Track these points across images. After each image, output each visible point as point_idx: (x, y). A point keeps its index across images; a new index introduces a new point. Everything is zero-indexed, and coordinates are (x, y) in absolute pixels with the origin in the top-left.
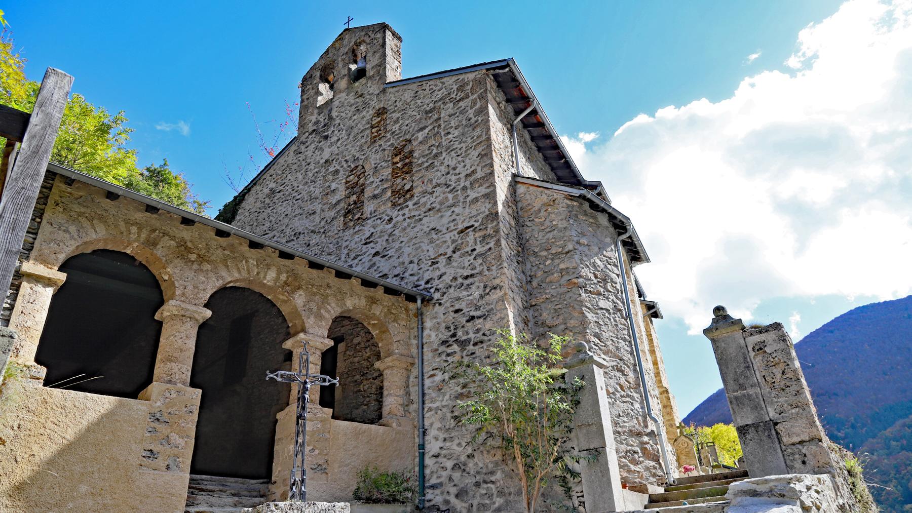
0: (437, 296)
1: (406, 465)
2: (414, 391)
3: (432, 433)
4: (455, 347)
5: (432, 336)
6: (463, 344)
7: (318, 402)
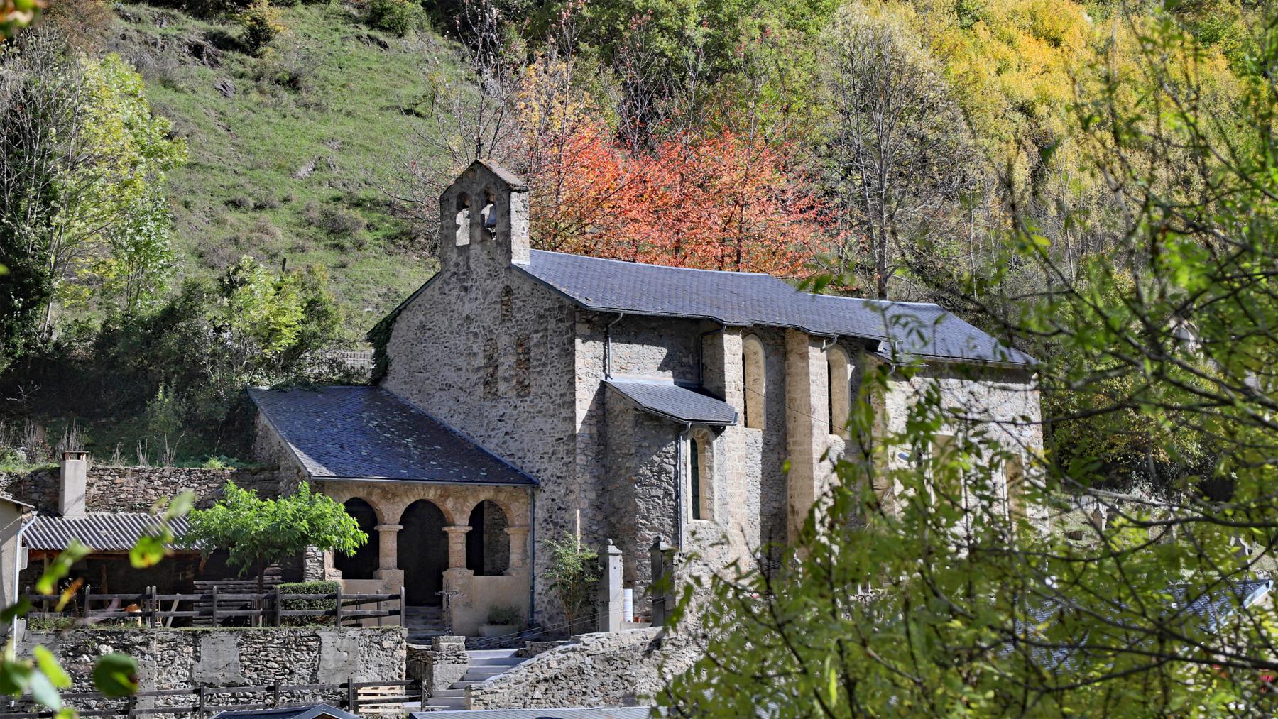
0: (542, 484)
1: (521, 600)
2: (529, 548)
3: (538, 580)
4: (551, 526)
5: (540, 514)
6: (555, 524)
7: (464, 563)
